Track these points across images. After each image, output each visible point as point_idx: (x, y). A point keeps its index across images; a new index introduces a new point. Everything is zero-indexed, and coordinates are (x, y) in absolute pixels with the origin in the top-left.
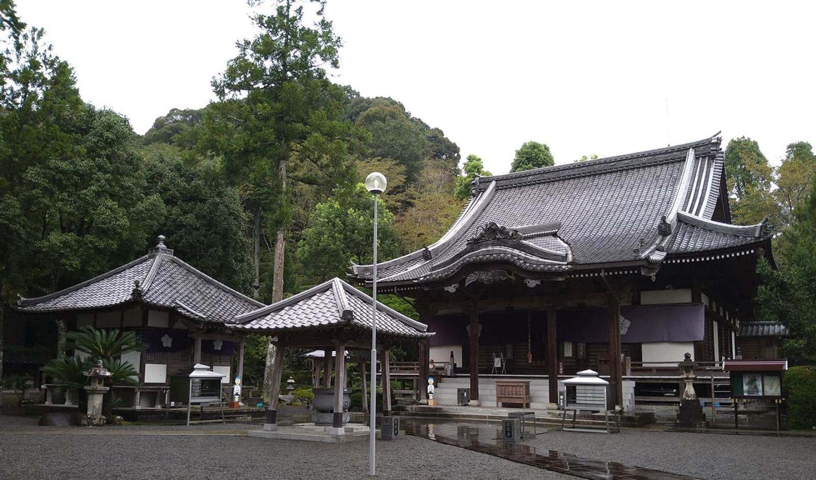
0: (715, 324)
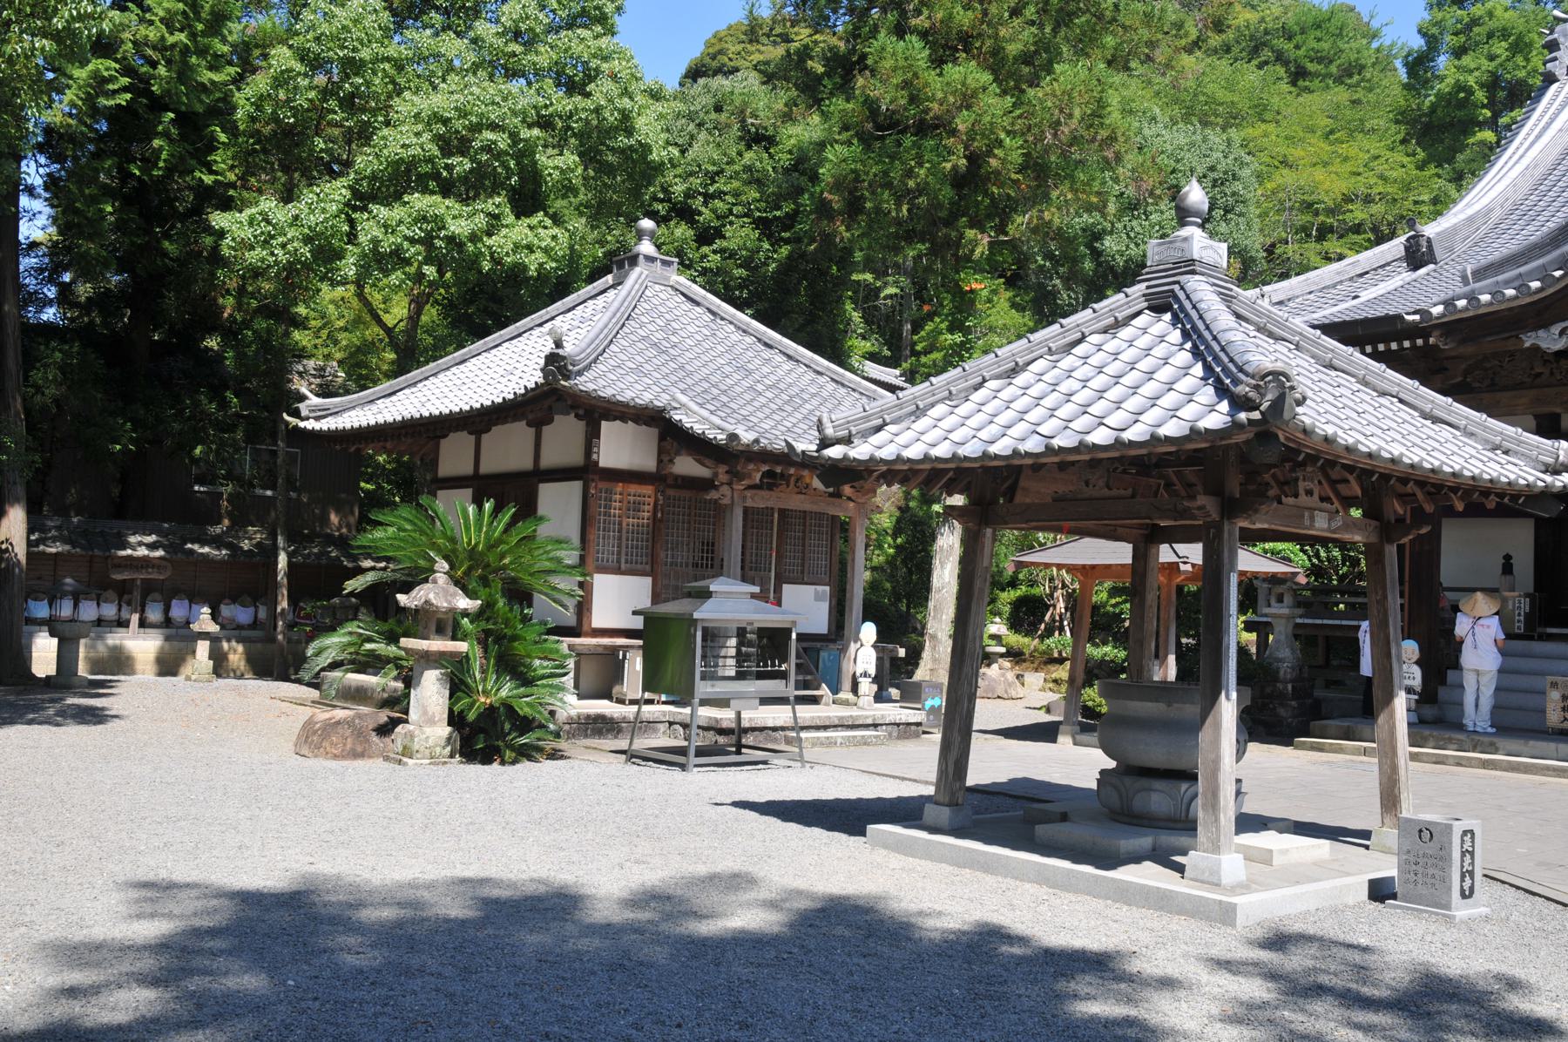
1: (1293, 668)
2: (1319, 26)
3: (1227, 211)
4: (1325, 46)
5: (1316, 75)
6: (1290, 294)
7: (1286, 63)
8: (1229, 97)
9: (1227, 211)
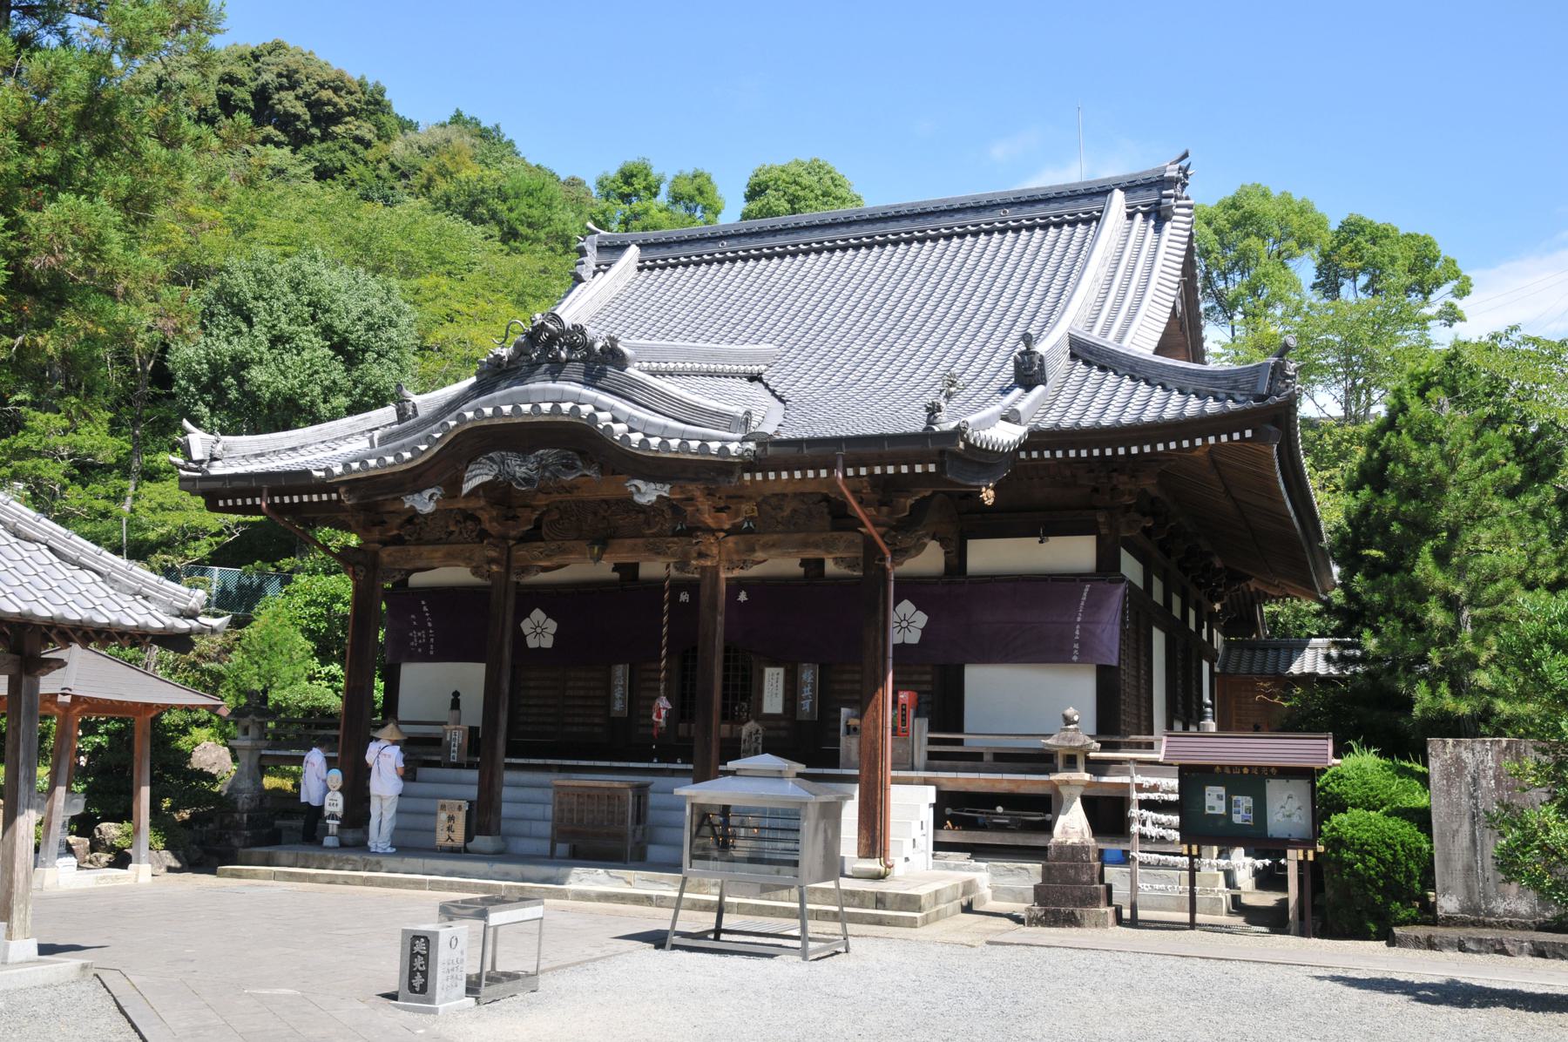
0: (1158, 638)
1: (252, 799)
2: (531, 194)
3: (380, 355)
4: (535, 213)
5: (527, 238)
6: (303, 441)
7: (500, 223)
8: (404, 246)
9: (380, 355)
